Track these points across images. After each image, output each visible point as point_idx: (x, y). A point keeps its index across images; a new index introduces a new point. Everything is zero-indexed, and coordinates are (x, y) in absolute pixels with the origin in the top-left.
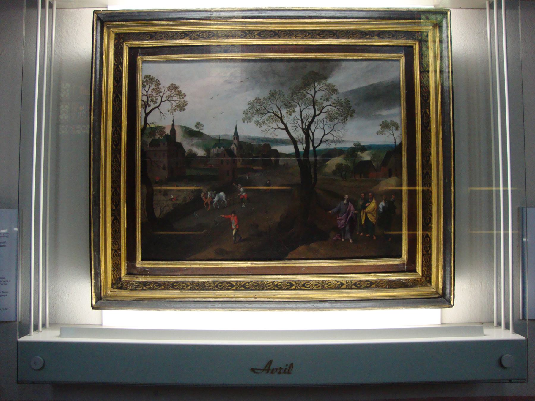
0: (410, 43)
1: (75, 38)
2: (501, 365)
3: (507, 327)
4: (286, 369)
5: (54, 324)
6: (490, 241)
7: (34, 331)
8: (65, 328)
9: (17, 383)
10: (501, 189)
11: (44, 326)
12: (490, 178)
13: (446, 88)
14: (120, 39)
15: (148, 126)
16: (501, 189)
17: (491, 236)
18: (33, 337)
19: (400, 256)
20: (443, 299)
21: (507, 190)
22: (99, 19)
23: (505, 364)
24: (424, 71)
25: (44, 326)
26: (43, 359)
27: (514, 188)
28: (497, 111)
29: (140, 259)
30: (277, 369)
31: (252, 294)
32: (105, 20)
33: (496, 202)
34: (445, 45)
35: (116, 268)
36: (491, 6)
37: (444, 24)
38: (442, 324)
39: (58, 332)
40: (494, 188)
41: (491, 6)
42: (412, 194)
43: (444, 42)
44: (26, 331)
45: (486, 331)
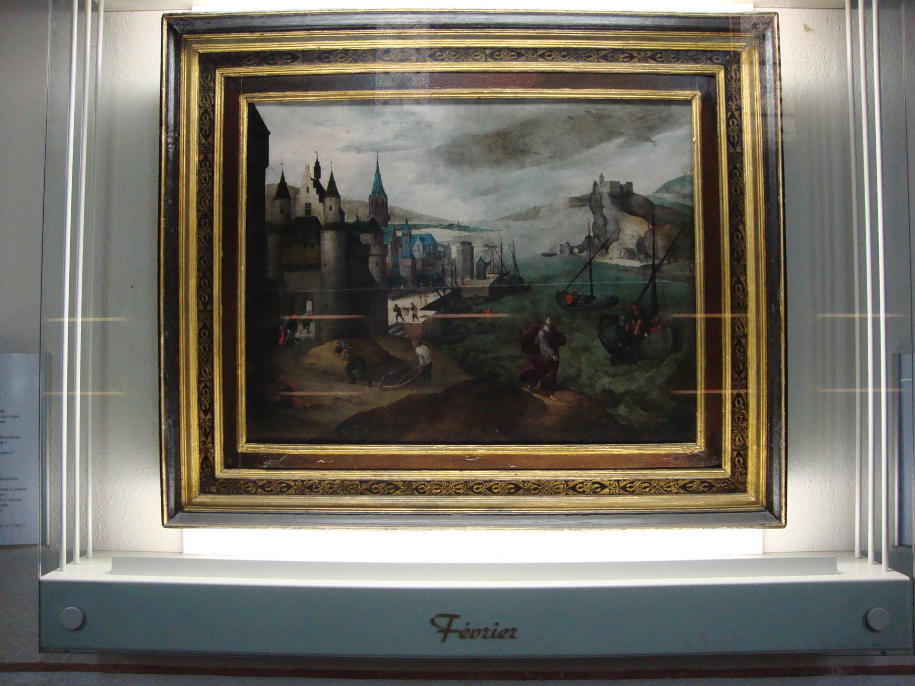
0: (707, 68)
1: (130, 64)
2: (869, 627)
3: (878, 559)
4: (495, 630)
5: (101, 551)
6: (850, 408)
7: (68, 562)
8: (121, 561)
9: (40, 651)
10: (79, 320)
11: (83, 553)
12: (850, 298)
13: (772, 147)
14: (209, 63)
15: (654, 394)
16: (79, 320)
17: (851, 397)
18: (67, 573)
19: (694, 440)
20: (770, 512)
21: (879, 319)
22: (170, 28)
23: (874, 625)
24: (735, 116)
25: (83, 553)
26: (78, 607)
27: (890, 315)
28: (852, 230)
29: (244, 440)
30: (479, 631)
31: (425, 503)
32: (181, 30)
33: (861, 341)
34: (769, 69)
35: (734, 95)
36: (854, 4)
37: (769, 34)
38: (764, 553)
39: (108, 566)
40: (857, 315)
41: (854, 4)
42: (714, 329)
43: (770, 85)
44: (53, 563)
45: (840, 566)
